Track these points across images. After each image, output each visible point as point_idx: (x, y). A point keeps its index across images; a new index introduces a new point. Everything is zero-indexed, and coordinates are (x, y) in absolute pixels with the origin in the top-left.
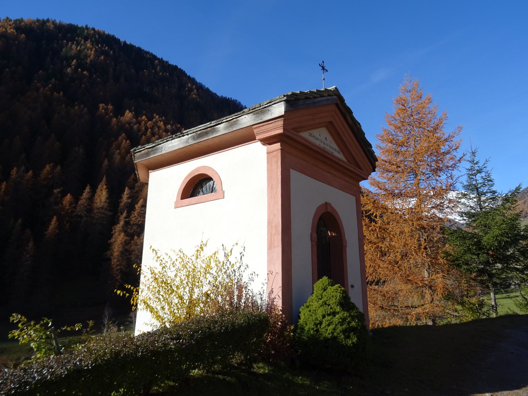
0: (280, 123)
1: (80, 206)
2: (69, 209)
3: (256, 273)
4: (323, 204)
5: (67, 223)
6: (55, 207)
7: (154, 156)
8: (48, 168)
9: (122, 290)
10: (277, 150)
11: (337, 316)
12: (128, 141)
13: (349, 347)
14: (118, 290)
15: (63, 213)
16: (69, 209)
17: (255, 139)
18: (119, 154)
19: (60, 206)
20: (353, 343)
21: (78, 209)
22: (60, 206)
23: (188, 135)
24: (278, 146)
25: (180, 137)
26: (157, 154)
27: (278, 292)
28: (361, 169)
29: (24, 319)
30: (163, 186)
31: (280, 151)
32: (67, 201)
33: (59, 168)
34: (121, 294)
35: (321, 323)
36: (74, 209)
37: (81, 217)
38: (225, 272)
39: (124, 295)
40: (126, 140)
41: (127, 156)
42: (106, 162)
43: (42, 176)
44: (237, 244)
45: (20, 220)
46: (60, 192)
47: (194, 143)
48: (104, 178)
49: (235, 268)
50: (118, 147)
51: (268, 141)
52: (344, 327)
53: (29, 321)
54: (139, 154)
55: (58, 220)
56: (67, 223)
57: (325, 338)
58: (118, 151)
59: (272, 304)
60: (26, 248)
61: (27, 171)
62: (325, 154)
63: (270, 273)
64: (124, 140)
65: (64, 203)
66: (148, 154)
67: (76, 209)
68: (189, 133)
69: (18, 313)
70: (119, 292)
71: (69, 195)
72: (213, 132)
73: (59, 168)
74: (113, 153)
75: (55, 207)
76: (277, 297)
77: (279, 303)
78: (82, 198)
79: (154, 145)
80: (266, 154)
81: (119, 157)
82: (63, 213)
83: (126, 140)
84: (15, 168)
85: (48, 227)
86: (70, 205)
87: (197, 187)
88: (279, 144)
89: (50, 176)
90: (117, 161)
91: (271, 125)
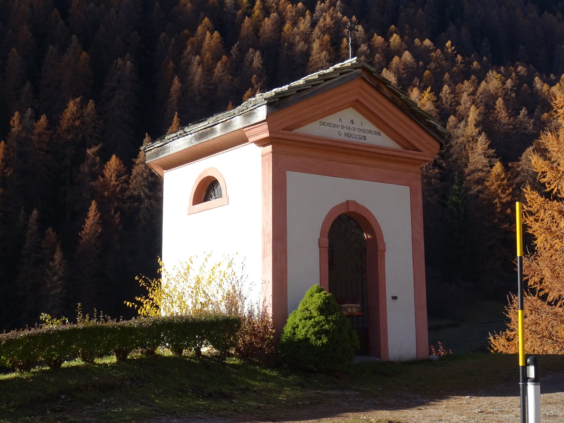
0: (265, 126)
1: (135, 177)
2: (118, 186)
3: (254, 283)
4: (342, 204)
5: (116, 213)
6: (93, 184)
7: (163, 156)
8: (72, 106)
9: (131, 302)
10: (269, 153)
11: (313, 320)
12: (216, 34)
13: (319, 346)
14: (127, 301)
15: (106, 193)
16: (118, 186)
17: (248, 141)
18: (200, 63)
19: (101, 180)
20: (323, 344)
21: (133, 183)
22: (101, 180)
23: (191, 134)
24: (269, 148)
25: (184, 136)
26: (165, 155)
27: (270, 300)
28: (419, 150)
29: (49, 317)
30: (178, 186)
31: (271, 154)
32: (112, 170)
33: (91, 104)
34: (131, 306)
35: (297, 327)
36: (125, 185)
37: (138, 199)
38: (231, 283)
39: (133, 306)
40: (212, 33)
41: (215, 67)
42: (176, 83)
43: (64, 124)
44: (237, 253)
45: (35, 212)
46: (97, 154)
47: (196, 143)
48: (176, 117)
49: (239, 278)
50: (198, 51)
51: (262, 143)
52: (316, 329)
53: (52, 318)
54: (149, 153)
55: (99, 208)
56: (116, 213)
57: (298, 339)
58: (198, 57)
59: (266, 312)
60: (51, 263)
61: (37, 118)
62: (340, 145)
63: (264, 282)
64: (208, 33)
65: (107, 174)
66: (157, 154)
67: (128, 184)
68: (191, 132)
69: (45, 312)
70: (128, 303)
71: (114, 156)
72: (212, 133)
73: (91, 104)
74: (189, 64)
75: (93, 184)
76: (269, 305)
77: (270, 311)
78: (137, 162)
79: (162, 144)
80: (261, 157)
81: (200, 70)
82: (106, 193)
83: (212, 33)
84: (17, 114)
85: (84, 223)
86: (118, 176)
87: (207, 190)
88: (271, 146)
89: (77, 123)
90: (197, 78)
91: (259, 129)
